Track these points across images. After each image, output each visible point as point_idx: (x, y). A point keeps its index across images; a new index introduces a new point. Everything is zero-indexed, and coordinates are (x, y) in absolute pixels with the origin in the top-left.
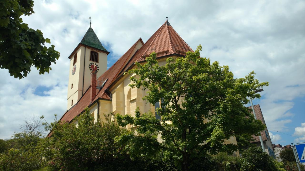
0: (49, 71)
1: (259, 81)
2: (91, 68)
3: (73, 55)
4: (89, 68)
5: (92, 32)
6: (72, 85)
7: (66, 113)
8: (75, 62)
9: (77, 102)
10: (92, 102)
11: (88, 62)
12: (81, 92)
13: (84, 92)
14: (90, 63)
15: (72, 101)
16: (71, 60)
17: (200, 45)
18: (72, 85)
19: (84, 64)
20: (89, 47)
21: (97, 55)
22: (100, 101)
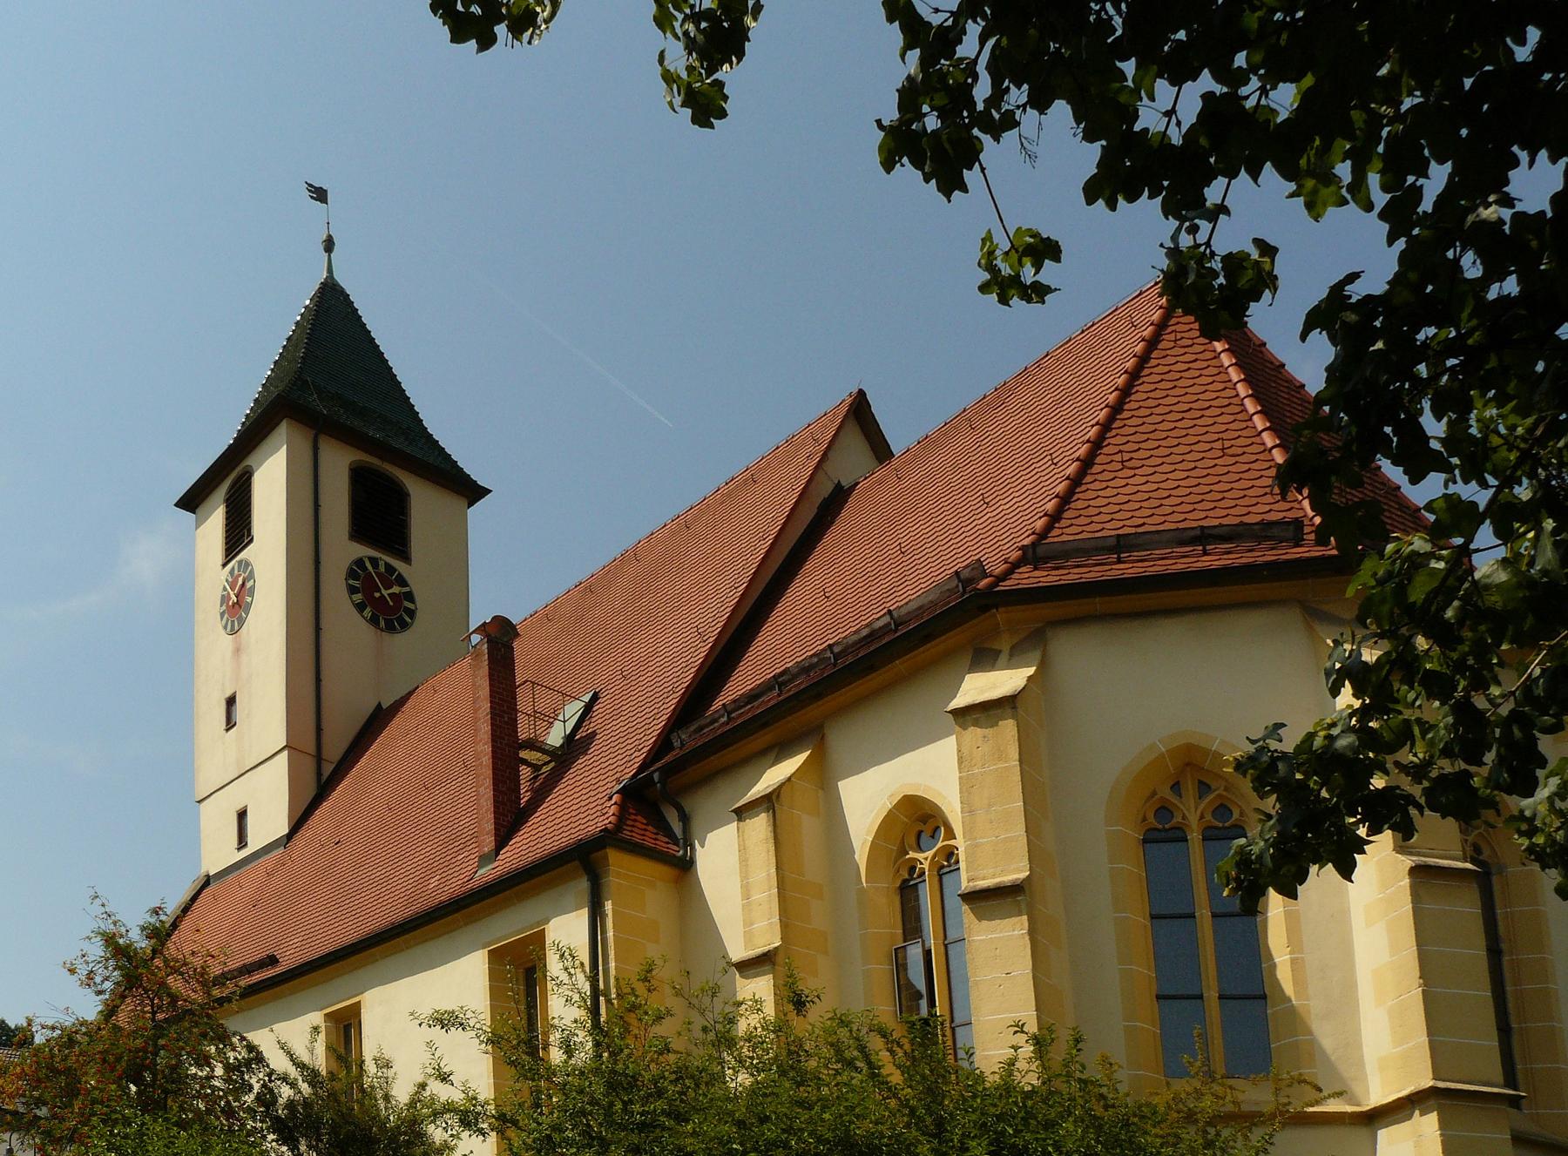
0: (1483, 523)
1: (1352, 277)
2: (358, 597)
3: (222, 480)
4: (413, 589)
5: (360, 326)
6: (231, 702)
7: (194, 899)
8: (238, 534)
9: (286, 831)
10: (502, 840)
11: (343, 550)
12: (309, 765)
13: (328, 769)
14: (355, 556)
15: (242, 815)
16: (198, 525)
17: (1259, 243)
18: (231, 702)
19: (317, 562)
20: (348, 436)
21: (400, 499)
22: (606, 858)
